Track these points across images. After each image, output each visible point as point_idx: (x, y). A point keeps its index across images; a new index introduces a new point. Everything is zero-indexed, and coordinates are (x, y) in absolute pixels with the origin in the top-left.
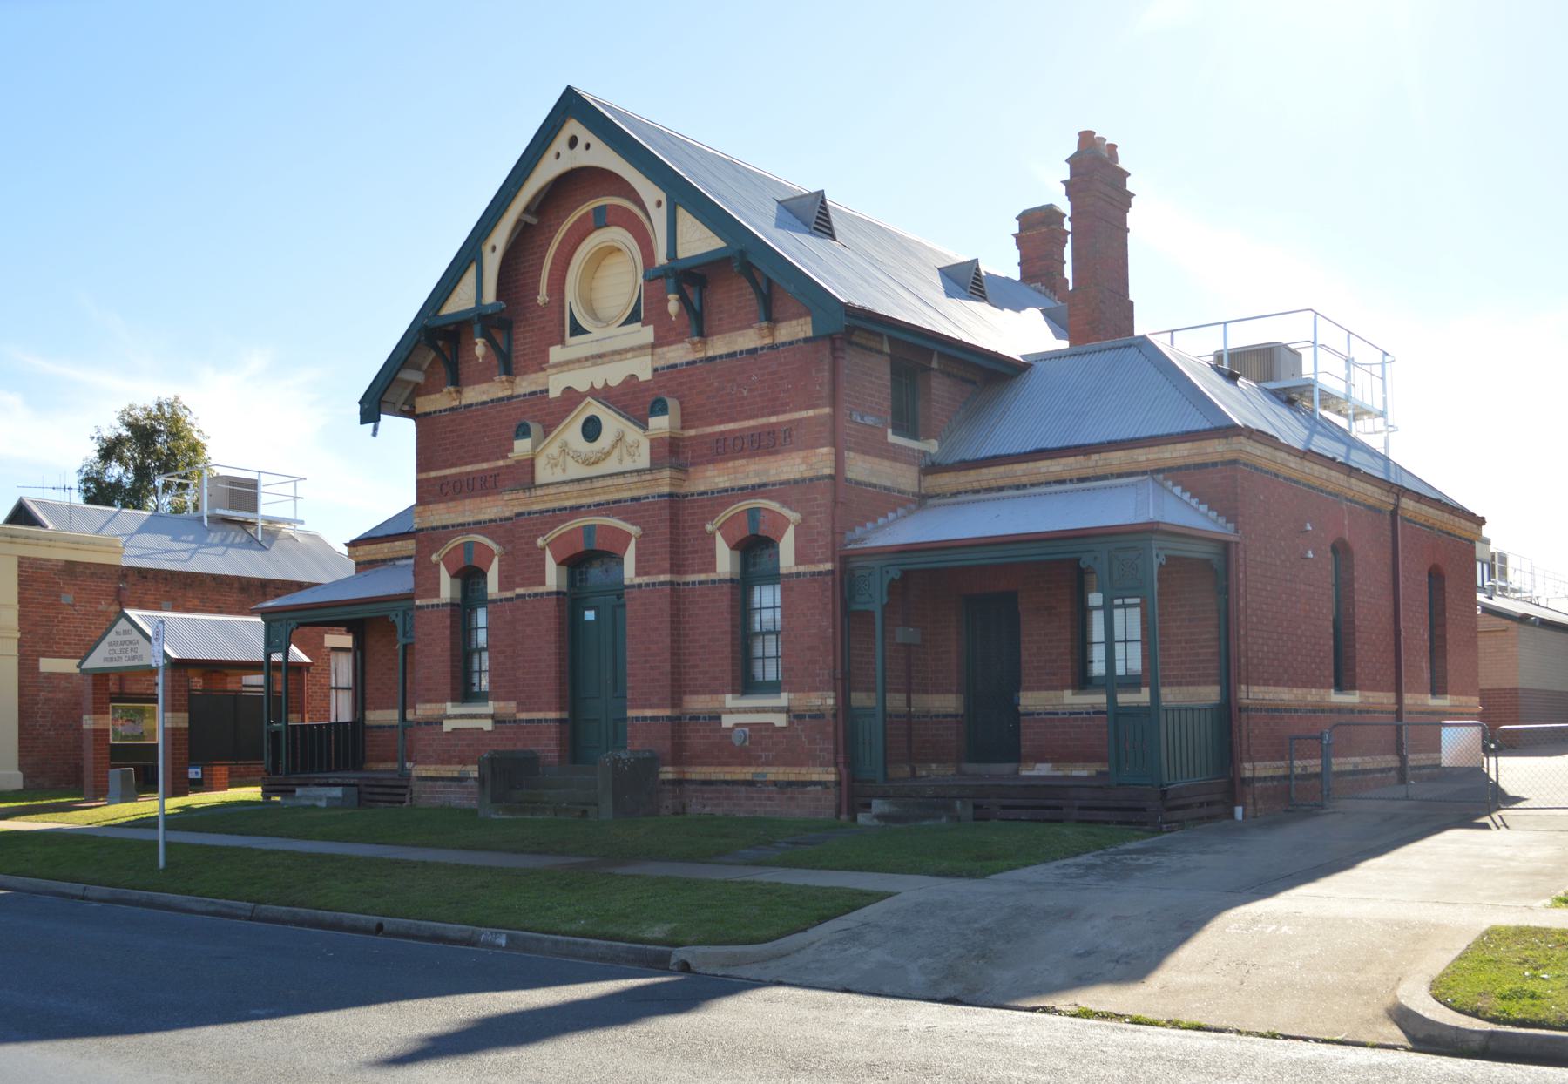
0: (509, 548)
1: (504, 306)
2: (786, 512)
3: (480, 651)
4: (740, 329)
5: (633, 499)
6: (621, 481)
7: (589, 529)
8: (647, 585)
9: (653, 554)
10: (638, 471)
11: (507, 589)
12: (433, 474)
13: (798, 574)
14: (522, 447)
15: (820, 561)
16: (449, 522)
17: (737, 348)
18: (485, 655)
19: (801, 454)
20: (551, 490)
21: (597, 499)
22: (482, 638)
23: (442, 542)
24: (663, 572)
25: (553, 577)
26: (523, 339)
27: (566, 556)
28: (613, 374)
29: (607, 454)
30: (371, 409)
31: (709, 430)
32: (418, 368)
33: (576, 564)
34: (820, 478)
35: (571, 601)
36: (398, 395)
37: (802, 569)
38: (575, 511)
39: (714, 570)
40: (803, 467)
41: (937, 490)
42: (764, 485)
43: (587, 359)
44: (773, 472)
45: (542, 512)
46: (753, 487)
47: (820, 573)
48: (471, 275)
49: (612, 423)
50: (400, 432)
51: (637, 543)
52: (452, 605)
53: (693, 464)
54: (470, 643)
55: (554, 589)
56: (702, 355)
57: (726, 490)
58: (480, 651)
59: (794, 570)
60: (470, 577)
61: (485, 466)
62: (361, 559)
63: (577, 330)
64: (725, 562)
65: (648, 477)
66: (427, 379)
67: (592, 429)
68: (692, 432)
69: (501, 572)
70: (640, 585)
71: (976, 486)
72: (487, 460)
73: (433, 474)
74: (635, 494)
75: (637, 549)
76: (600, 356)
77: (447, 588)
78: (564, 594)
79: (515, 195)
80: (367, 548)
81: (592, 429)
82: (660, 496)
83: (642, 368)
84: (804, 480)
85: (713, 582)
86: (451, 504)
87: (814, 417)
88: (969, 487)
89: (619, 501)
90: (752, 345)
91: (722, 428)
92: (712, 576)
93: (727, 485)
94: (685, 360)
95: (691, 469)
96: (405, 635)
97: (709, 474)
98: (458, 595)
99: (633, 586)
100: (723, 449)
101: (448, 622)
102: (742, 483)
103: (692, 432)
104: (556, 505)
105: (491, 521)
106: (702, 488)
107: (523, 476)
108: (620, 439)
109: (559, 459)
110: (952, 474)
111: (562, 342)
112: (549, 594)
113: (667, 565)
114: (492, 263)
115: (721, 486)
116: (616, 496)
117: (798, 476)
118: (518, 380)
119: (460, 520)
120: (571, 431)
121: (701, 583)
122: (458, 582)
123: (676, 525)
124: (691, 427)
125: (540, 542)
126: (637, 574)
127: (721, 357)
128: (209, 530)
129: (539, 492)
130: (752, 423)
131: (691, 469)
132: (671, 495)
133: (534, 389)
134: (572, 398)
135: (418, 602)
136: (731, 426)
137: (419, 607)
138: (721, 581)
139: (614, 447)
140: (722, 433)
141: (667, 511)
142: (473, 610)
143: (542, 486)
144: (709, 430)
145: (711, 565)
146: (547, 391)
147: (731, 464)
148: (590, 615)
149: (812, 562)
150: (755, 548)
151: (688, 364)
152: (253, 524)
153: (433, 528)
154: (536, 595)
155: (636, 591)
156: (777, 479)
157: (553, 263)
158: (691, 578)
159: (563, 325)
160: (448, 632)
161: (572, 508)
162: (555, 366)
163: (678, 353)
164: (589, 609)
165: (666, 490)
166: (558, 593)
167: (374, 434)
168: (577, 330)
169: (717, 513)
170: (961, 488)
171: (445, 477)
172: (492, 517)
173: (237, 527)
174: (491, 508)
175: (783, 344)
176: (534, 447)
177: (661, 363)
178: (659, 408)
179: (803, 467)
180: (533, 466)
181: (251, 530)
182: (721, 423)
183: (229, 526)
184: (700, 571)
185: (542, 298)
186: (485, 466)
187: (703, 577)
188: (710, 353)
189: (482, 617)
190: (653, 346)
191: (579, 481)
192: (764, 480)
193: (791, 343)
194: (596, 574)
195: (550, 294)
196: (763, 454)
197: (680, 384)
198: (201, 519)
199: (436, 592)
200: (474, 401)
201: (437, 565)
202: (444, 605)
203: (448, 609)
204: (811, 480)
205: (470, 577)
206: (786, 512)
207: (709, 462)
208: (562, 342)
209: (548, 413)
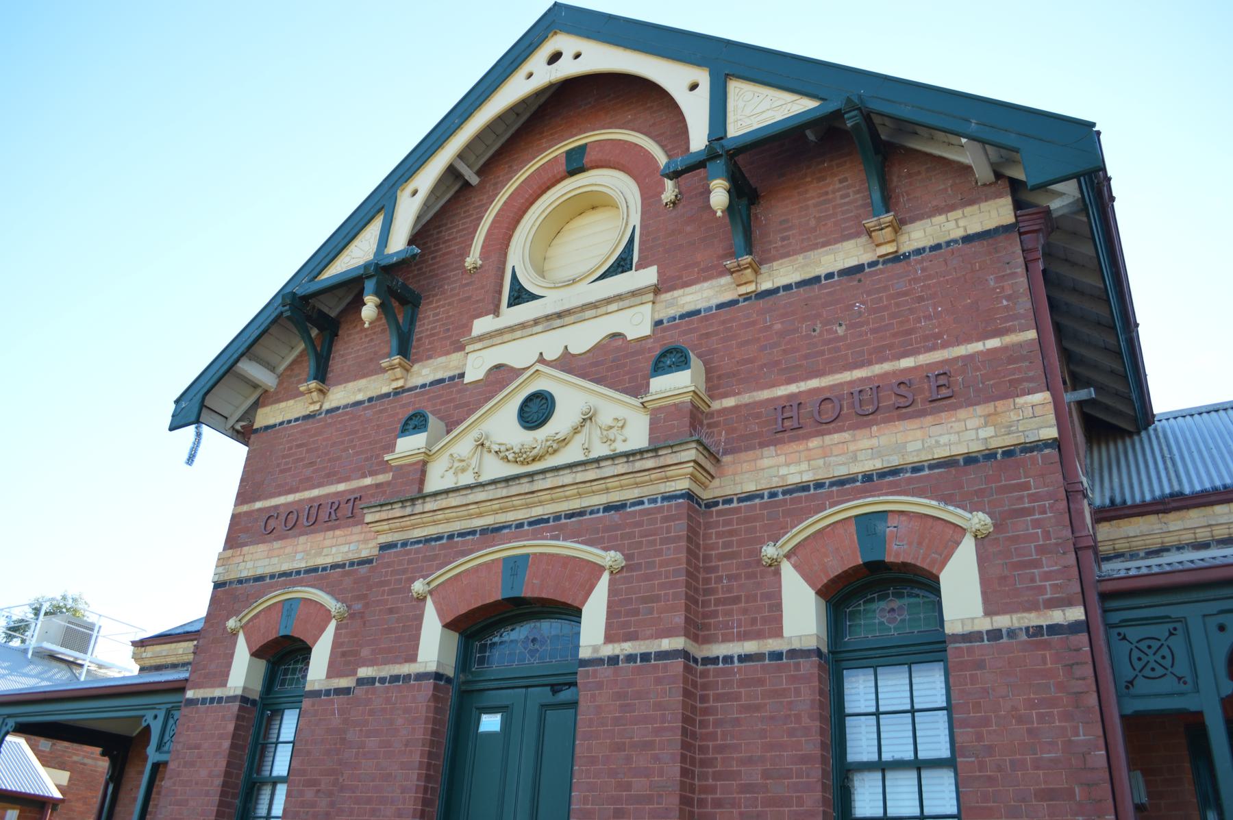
0: (358, 606)
1: (417, 250)
2: (953, 514)
3: (275, 782)
4: (824, 245)
5: (608, 508)
6: (591, 474)
7: (515, 565)
8: (630, 658)
9: (645, 600)
10: (628, 455)
11: (340, 675)
12: (258, 505)
13: (995, 634)
14: (409, 445)
15: (1052, 604)
16: (268, 570)
17: (821, 271)
18: (282, 790)
19: (980, 410)
20: (454, 500)
21: (537, 512)
22: (281, 764)
23: (249, 600)
24: (669, 633)
25: (433, 647)
26: (431, 318)
27: (448, 620)
28: (582, 338)
29: (564, 442)
30: (194, 408)
31: (765, 394)
32: (272, 369)
33: (475, 628)
34: (1028, 448)
35: (460, 694)
36: (233, 402)
37: (1003, 622)
38: (492, 533)
39: (778, 633)
40: (987, 432)
41: (1121, 546)
42: (894, 472)
43: (536, 322)
44: (910, 447)
45: (428, 540)
46: (868, 477)
47: (1053, 629)
48: (372, 232)
49: (573, 399)
50: (225, 457)
51: (612, 583)
52: (244, 699)
53: (726, 453)
54: (259, 771)
55: (432, 668)
56: (751, 288)
57: (804, 488)
58: (275, 782)
59: (985, 625)
60: (283, 655)
61: (341, 487)
62: (148, 663)
63: (520, 295)
64: (802, 616)
65: (650, 463)
66: (280, 384)
67: (536, 410)
68: (729, 402)
69: (336, 644)
70: (613, 660)
71: (1203, 535)
72: (346, 479)
73: (258, 505)
74: (615, 497)
75: (612, 592)
76: (559, 315)
77: (242, 672)
78: (449, 680)
79: (459, 127)
80: (158, 648)
81: (536, 410)
82: (667, 498)
83: (636, 323)
84: (990, 455)
85: (776, 656)
86: (277, 545)
87: (1004, 349)
88: (1187, 537)
89: (581, 513)
90: (852, 262)
91: (793, 388)
92: (772, 645)
93: (807, 477)
94: (715, 302)
95: (726, 459)
96: (159, 747)
97: (766, 462)
98: (257, 687)
99: (599, 661)
100: (789, 424)
101: (231, 727)
102: (842, 471)
103: (729, 402)
104: (457, 526)
105: (334, 566)
106: (751, 487)
107: (410, 487)
108: (588, 418)
109: (468, 458)
110: (1152, 518)
111: (496, 312)
112: (420, 677)
113: (679, 619)
114: (408, 210)
115: (794, 479)
116: (575, 504)
117: (975, 447)
118: (416, 367)
119: (285, 567)
120: (501, 422)
121: (744, 658)
122: (262, 665)
123: (701, 555)
124: (725, 395)
125: (418, 586)
126: (609, 639)
127: (787, 287)
128: (31, 662)
129: (430, 505)
130: (814, 383)
131: (726, 459)
132: (689, 496)
133: (439, 376)
134: (501, 376)
135: (190, 694)
136: (814, 383)
137: (191, 702)
138: (793, 653)
139: (576, 431)
140: (791, 396)
141: (683, 523)
142: (278, 713)
143: (435, 494)
144: (765, 394)
145: (773, 623)
146: (462, 375)
147: (814, 443)
148: (490, 723)
149: (1032, 607)
150: (877, 592)
151: (720, 306)
152: (81, 666)
153: (240, 581)
154: (395, 678)
155: (605, 672)
156: (925, 456)
157: (494, 222)
158: (719, 650)
159: (500, 293)
160: (226, 744)
161: (484, 531)
162: (480, 338)
163: (701, 295)
164: (491, 710)
165: (683, 485)
166: (438, 676)
167: (191, 459)
168: (520, 295)
169: (784, 529)
170: (1170, 540)
171: (276, 507)
172: (338, 559)
173: (63, 666)
174: (337, 547)
175: (919, 251)
176: (430, 444)
177: (665, 313)
178: (670, 358)
179: (987, 432)
180: (423, 473)
181: (77, 671)
182: (790, 381)
183: (54, 663)
184: (744, 636)
185: (473, 258)
186: (341, 487)
187: (750, 647)
188: (766, 285)
189: (288, 726)
190: (657, 290)
191: (507, 480)
192: (895, 461)
193: (937, 247)
194: (515, 645)
195: (484, 254)
196: (887, 421)
197: (708, 335)
198: (25, 651)
199: (222, 677)
200: (343, 402)
201: (234, 634)
202: (231, 699)
203: (235, 706)
204: (1009, 453)
205: (283, 655)
206: (953, 514)
207: (763, 445)
208: (496, 312)
209: (455, 403)
